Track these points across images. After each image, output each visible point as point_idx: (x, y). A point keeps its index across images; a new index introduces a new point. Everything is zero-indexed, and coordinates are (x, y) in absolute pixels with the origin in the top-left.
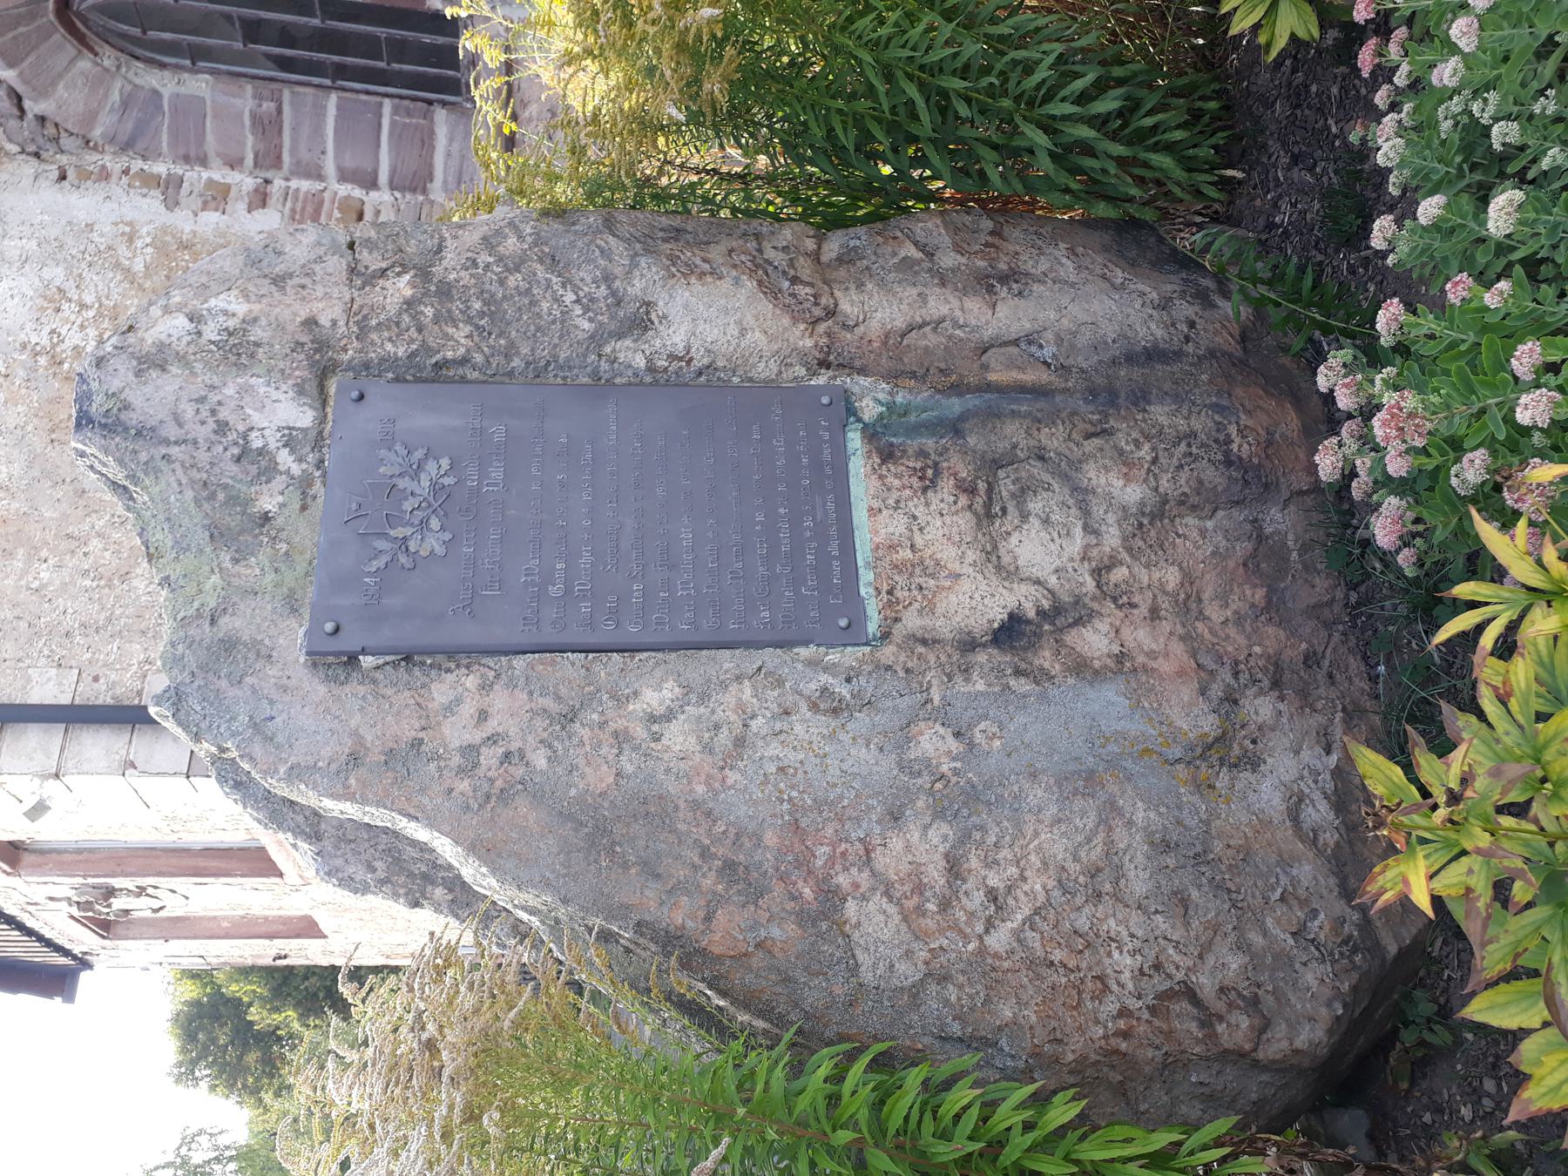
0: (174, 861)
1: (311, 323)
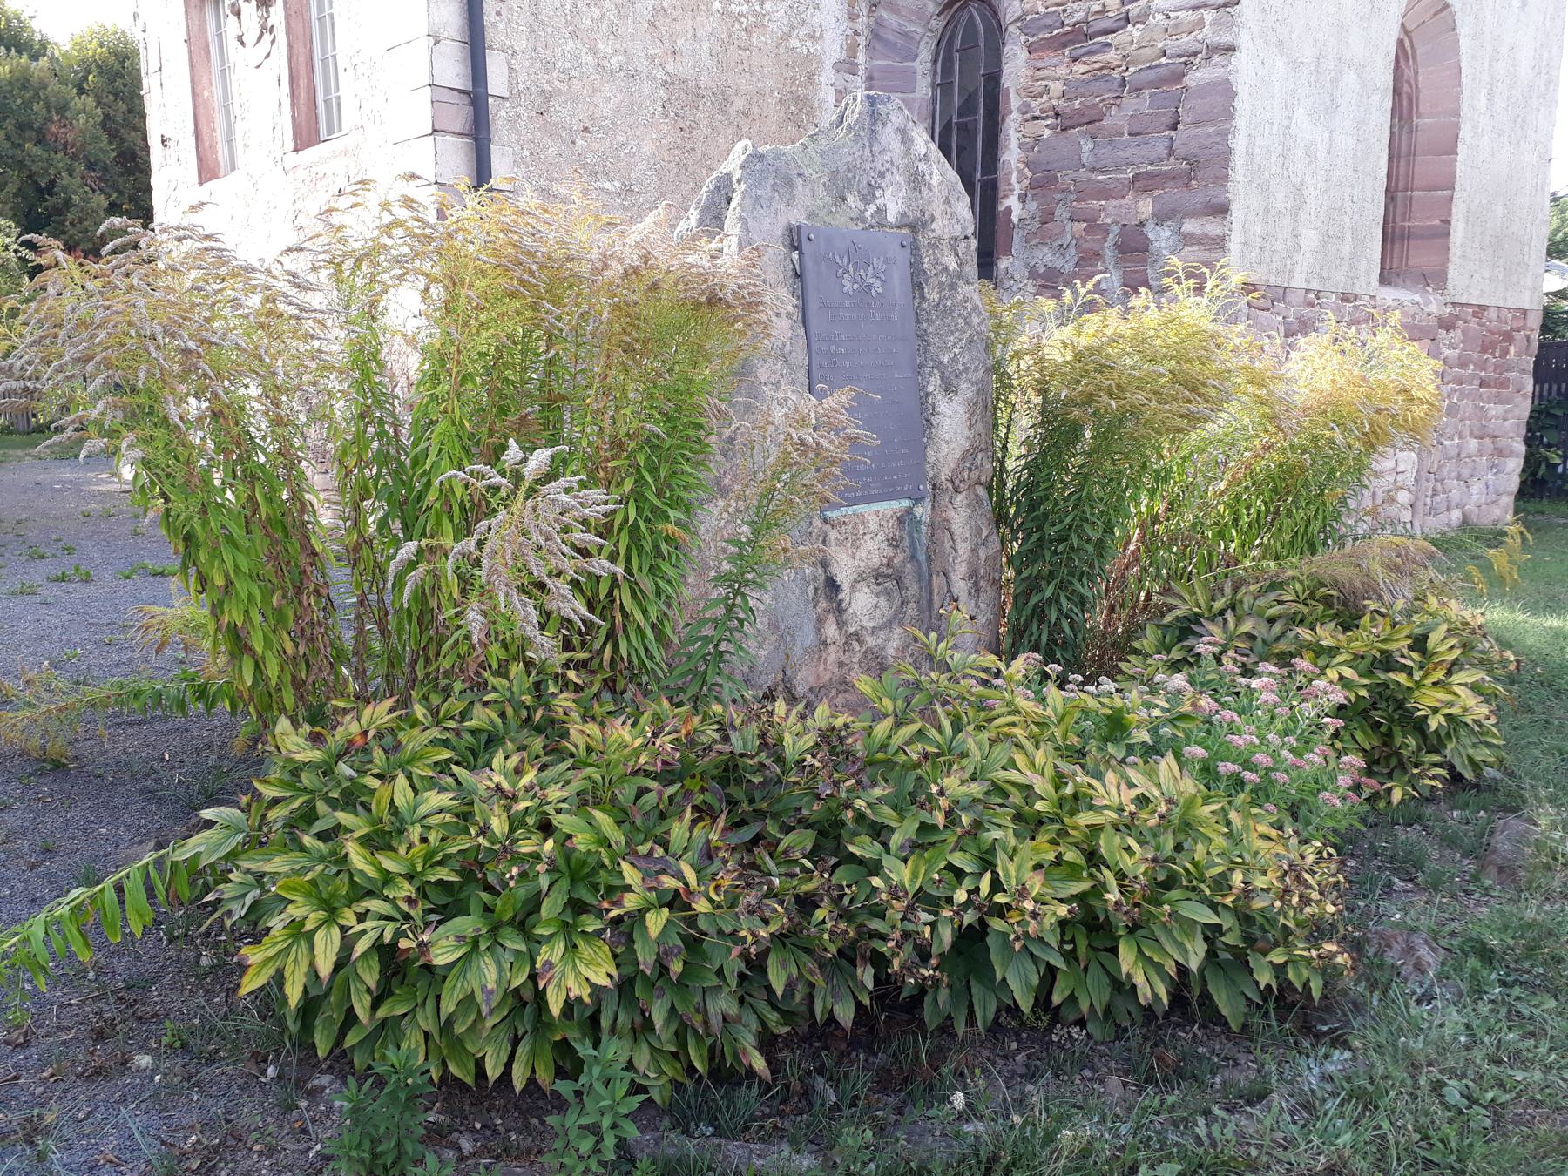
0: (302, 59)
1: (933, 219)
